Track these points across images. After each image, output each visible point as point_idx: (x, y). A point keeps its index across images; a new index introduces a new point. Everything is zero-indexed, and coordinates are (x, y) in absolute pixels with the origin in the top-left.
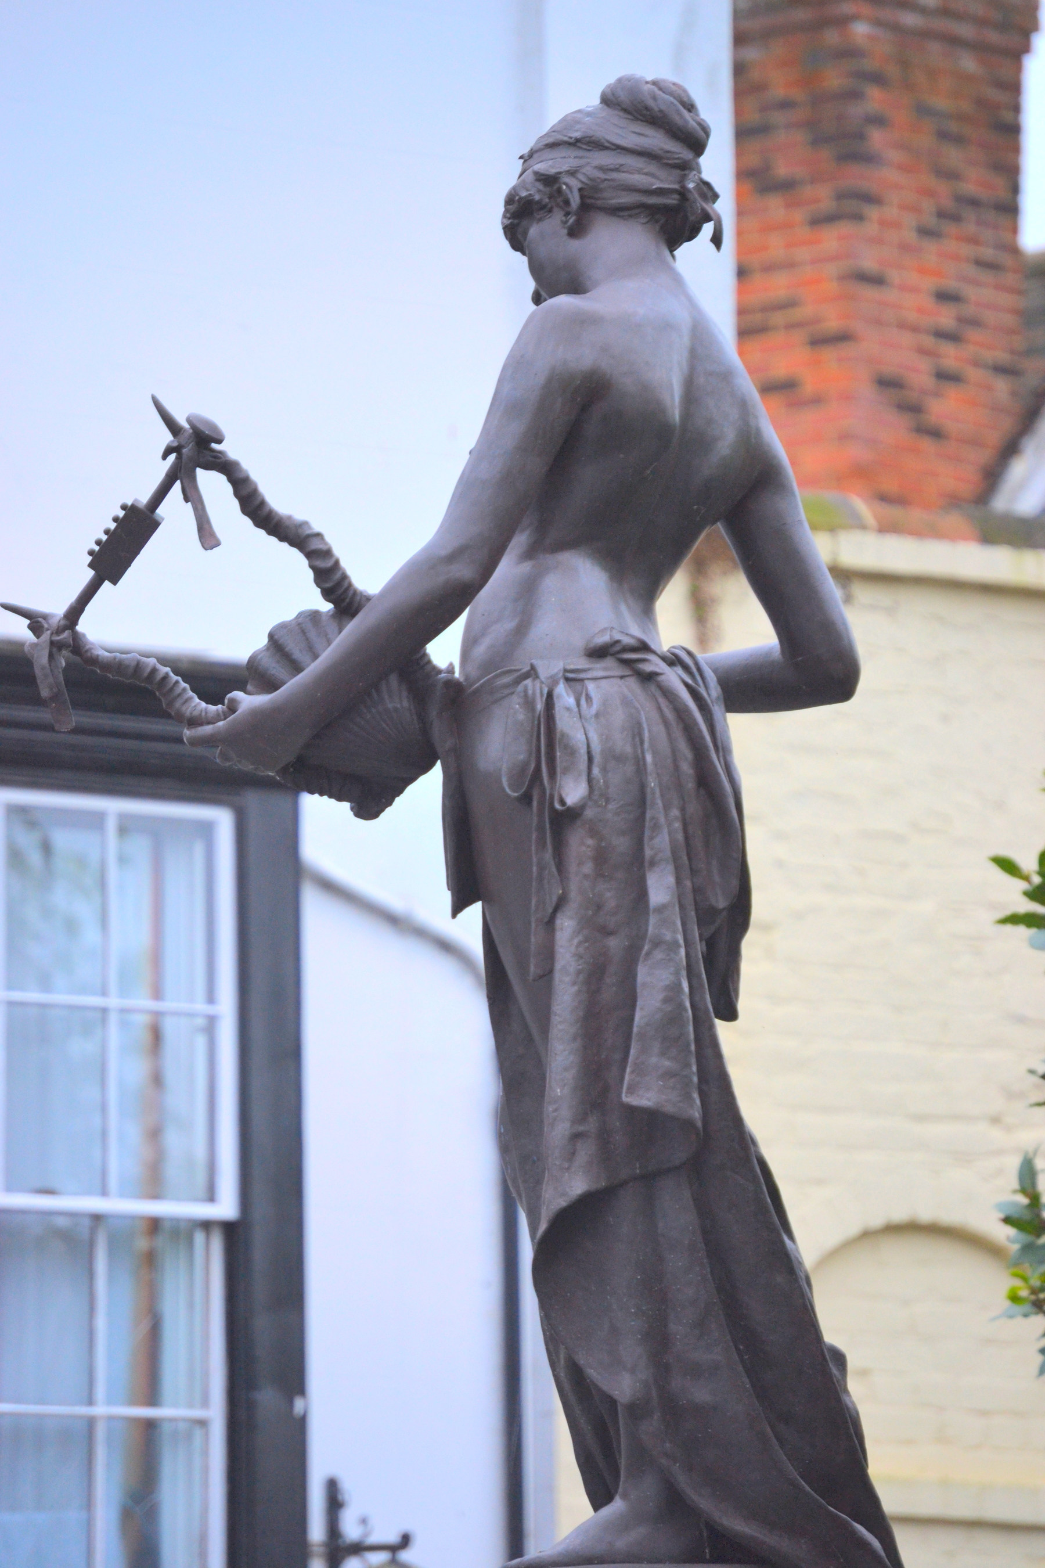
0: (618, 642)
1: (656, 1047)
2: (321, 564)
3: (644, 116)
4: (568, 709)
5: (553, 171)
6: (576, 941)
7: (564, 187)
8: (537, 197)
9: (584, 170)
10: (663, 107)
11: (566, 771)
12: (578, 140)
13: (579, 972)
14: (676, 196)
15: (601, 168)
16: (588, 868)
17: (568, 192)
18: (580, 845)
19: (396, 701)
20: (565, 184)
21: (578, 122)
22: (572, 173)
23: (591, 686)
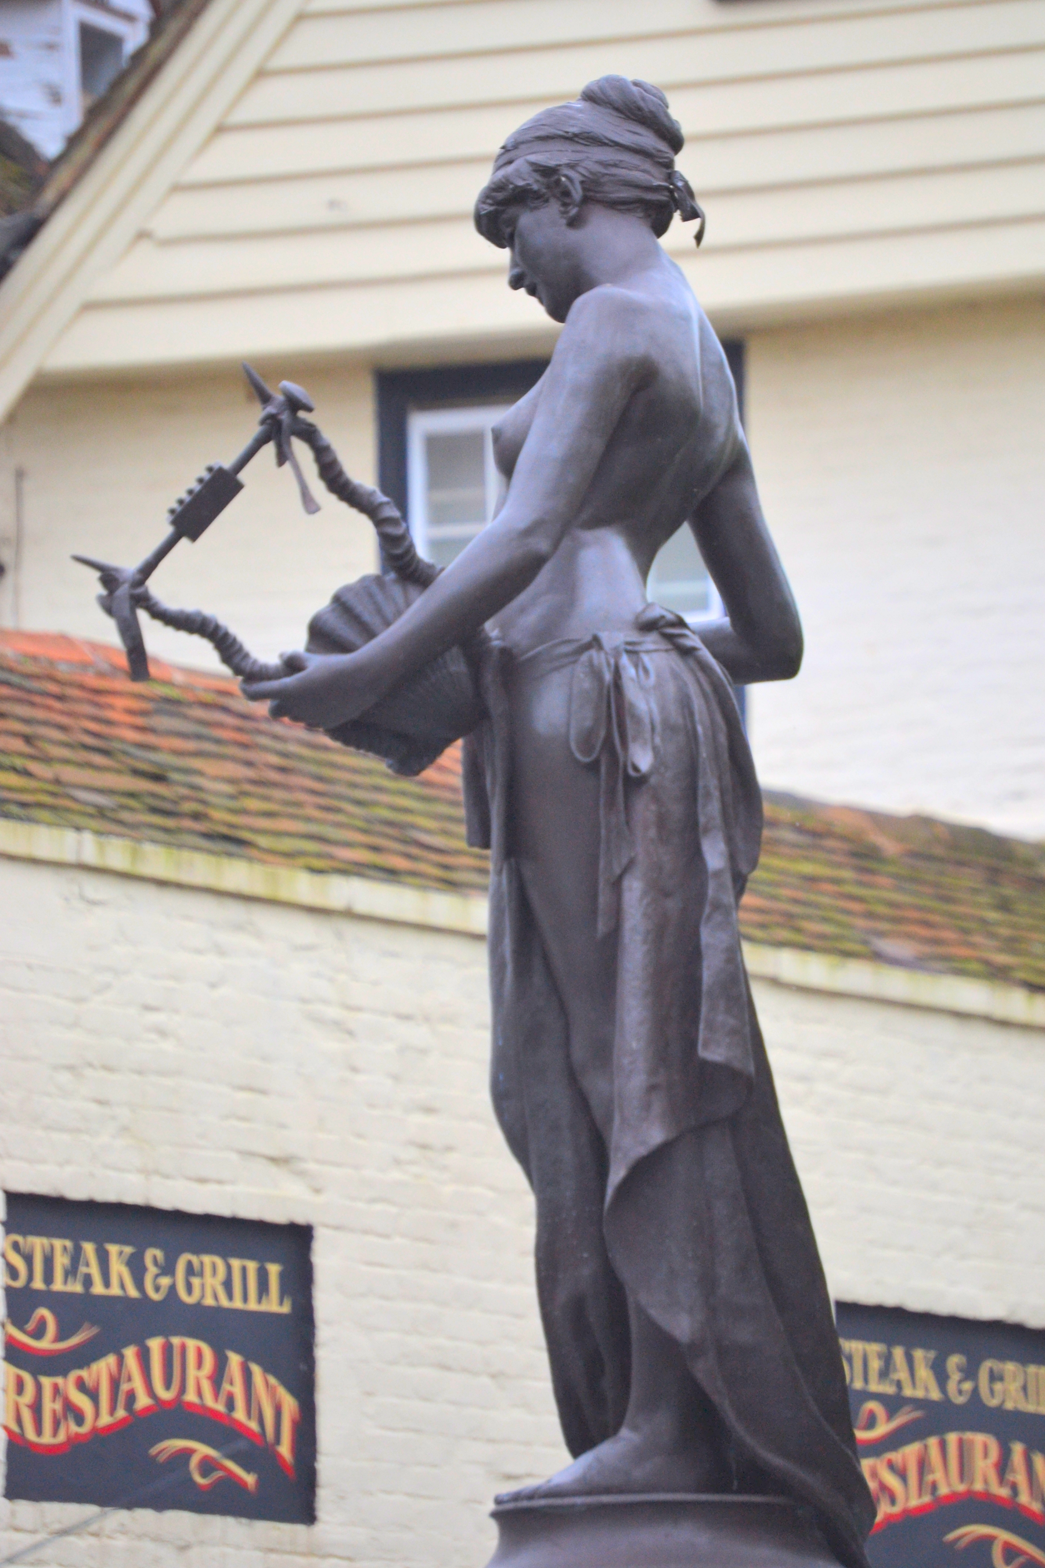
0: (663, 617)
1: (722, 1005)
2: (391, 530)
3: (634, 115)
4: (632, 680)
5: (552, 163)
6: (645, 901)
7: (563, 179)
8: (535, 187)
9: (584, 164)
10: (653, 109)
11: (635, 739)
12: (576, 135)
13: (648, 932)
14: (667, 194)
15: (601, 163)
16: (652, 833)
17: (568, 183)
18: (644, 809)
19: (456, 665)
20: (566, 176)
21: (571, 118)
22: (572, 166)
23: (646, 658)
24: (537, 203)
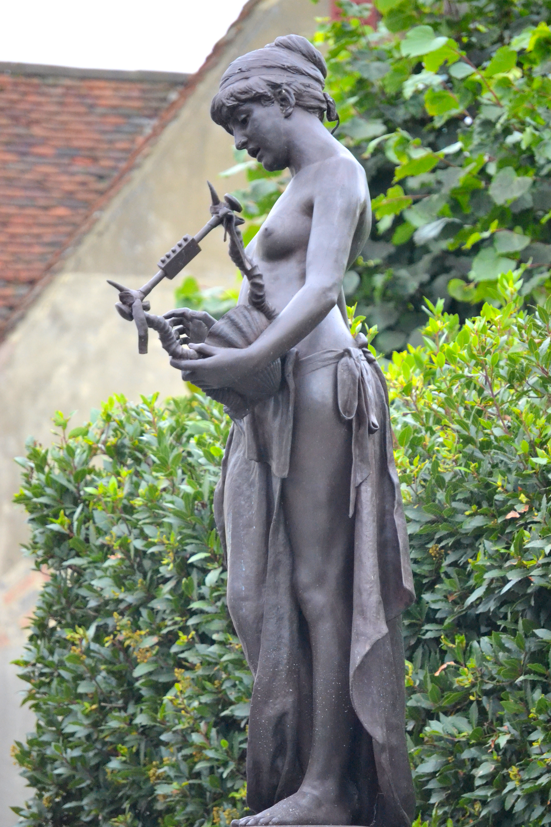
5: (279, 82)
7: (284, 91)
8: (269, 94)
9: (295, 84)
12: (289, 67)
15: (303, 85)
22: (288, 85)
24: (267, 103)
